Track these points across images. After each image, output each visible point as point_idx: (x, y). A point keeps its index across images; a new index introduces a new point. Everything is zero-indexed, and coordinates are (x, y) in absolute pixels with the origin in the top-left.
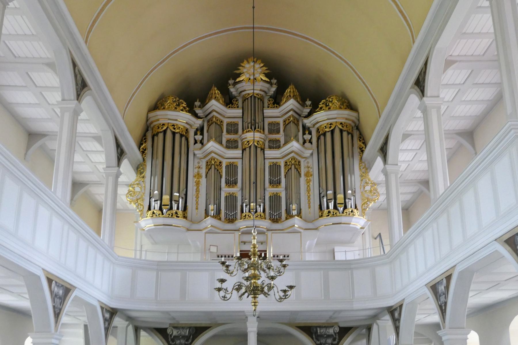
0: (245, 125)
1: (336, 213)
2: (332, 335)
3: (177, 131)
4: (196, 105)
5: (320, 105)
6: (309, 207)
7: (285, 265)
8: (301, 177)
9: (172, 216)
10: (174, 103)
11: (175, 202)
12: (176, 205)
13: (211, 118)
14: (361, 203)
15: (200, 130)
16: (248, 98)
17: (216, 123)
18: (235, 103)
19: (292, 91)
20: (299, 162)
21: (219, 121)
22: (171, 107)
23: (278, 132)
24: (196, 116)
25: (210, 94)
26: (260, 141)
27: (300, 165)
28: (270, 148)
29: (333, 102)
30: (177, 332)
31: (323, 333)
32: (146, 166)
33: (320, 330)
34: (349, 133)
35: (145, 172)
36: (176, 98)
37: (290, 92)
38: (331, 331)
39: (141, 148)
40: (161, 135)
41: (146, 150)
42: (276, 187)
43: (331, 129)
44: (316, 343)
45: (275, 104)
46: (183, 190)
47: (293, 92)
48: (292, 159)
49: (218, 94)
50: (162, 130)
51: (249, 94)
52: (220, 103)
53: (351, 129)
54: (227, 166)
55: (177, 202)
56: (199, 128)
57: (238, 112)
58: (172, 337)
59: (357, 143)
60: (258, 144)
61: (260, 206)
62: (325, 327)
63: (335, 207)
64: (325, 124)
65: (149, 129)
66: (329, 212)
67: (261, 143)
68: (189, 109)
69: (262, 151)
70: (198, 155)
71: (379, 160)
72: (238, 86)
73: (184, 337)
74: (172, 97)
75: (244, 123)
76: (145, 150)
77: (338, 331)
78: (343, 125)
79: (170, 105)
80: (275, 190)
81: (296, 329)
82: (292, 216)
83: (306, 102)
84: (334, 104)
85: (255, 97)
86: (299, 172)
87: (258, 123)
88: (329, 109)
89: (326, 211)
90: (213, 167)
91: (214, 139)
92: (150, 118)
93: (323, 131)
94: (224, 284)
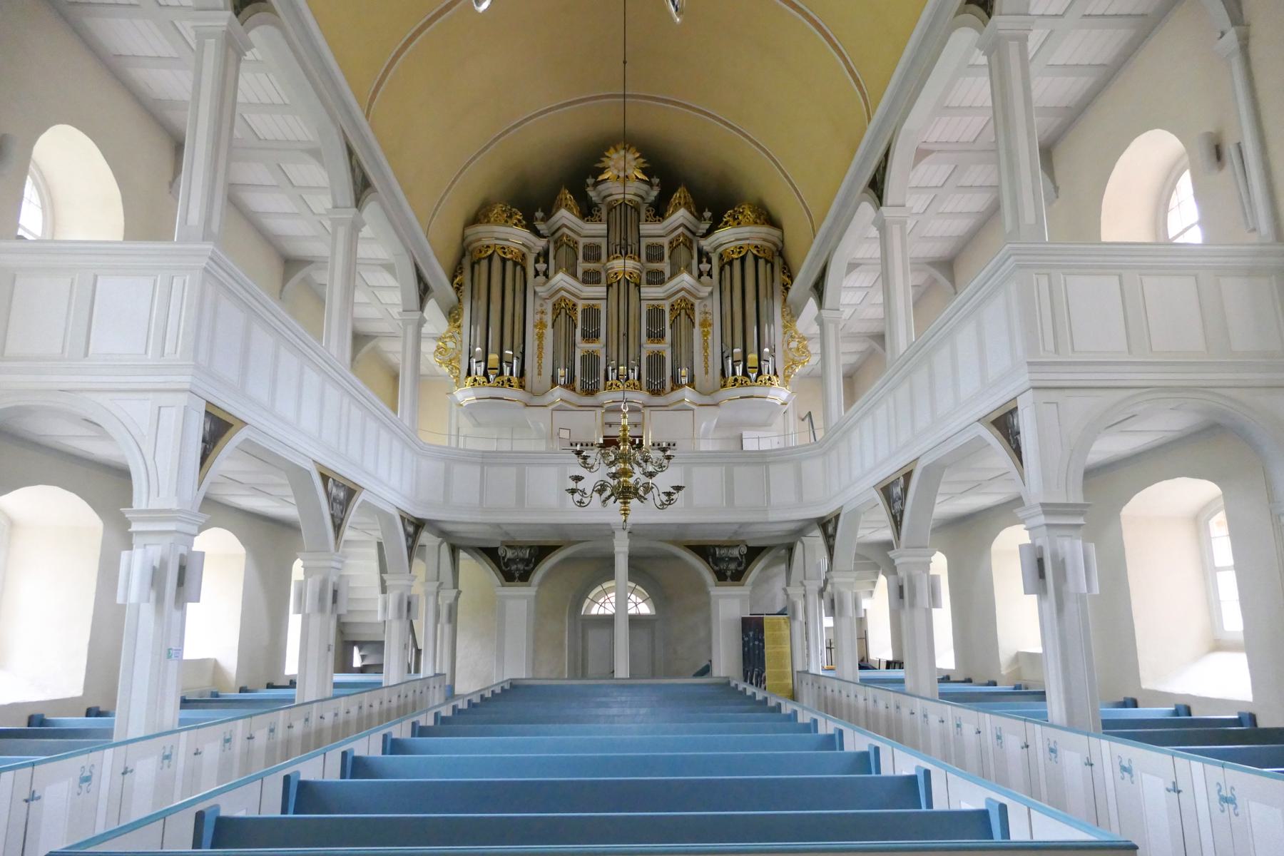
0: (612, 248)
1: (746, 382)
2: (737, 558)
3: (509, 256)
6: (707, 373)
9: (502, 385)
12: (508, 368)
13: (559, 238)
15: (544, 256)
17: (567, 245)
19: (682, 196)
23: (661, 259)
24: (537, 233)
28: (650, 283)
29: (745, 213)
30: (513, 554)
32: (463, 310)
34: (767, 261)
37: (680, 197)
38: (735, 553)
39: (455, 281)
40: (484, 263)
43: (741, 255)
46: (519, 347)
47: (685, 197)
48: (681, 301)
49: (571, 200)
50: (485, 255)
52: (573, 213)
54: (584, 311)
55: (510, 364)
56: (542, 252)
57: (600, 228)
58: (506, 560)
59: (779, 277)
60: (630, 277)
61: (633, 370)
63: (745, 373)
65: (467, 253)
66: (736, 380)
71: (812, 303)
72: (600, 187)
73: (522, 560)
74: (500, 203)
76: (461, 285)
79: (497, 217)
80: (655, 347)
82: (681, 386)
83: (704, 214)
85: (626, 204)
86: (691, 320)
88: (739, 224)
89: (731, 379)
90: (563, 311)
94: (579, 483)
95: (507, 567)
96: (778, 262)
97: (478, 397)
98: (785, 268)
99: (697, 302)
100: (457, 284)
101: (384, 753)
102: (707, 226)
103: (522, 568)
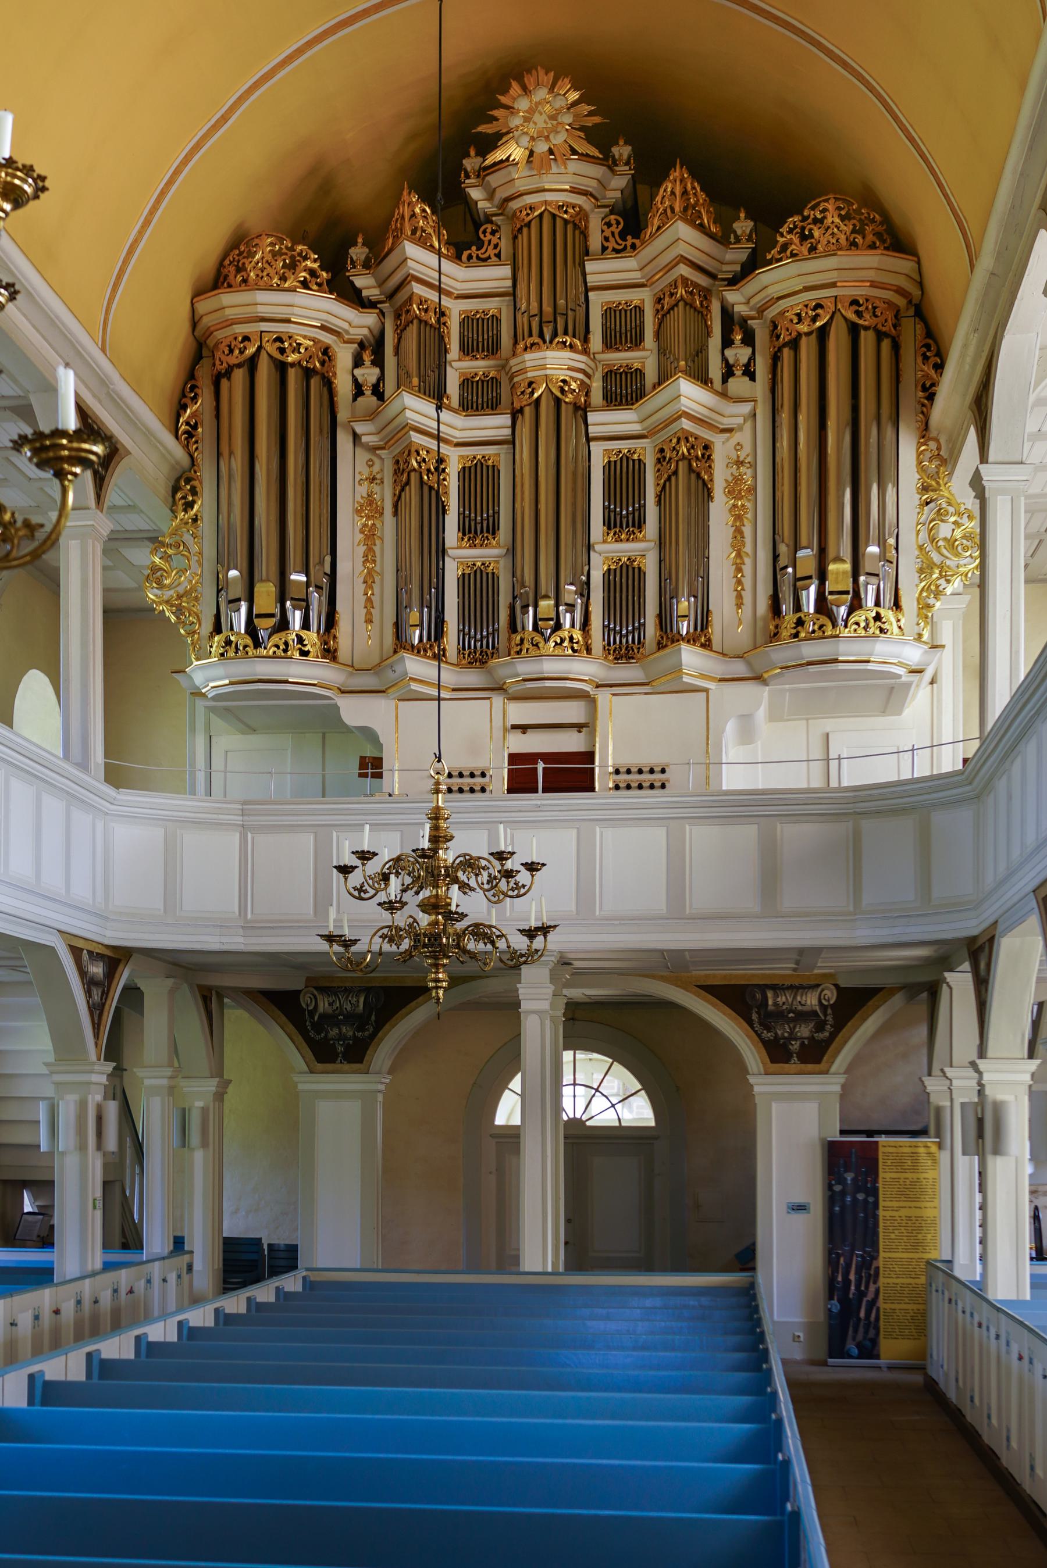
0: (522, 320)
2: (814, 1013)
3: (292, 358)
4: (355, 258)
5: (782, 235)
7: (512, 871)
8: (712, 498)
10: (276, 260)
11: (294, 602)
12: (298, 613)
14: (917, 586)
16: (530, 221)
17: (420, 321)
18: (490, 242)
19: (678, 190)
20: (706, 447)
21: (432, 314)
22: (268, 275)
23: (637, 341)
24: (354, 298)
25: (397, 219)
26: (572, 378)
27: (709, 456)
29: (829, 220)
30: (330, 1004)
31: (784, 1007)
33: (776, 996)
35: (199, 503)
36: (281, 240)
37: (673, 193)
38: (811, 1000)
39: (181, 420)
40: (239, 376)
41: (199, 426)
42: (628, 540)
43: (818, 324)
44: (759, 1036)
45: (629, 238)
47: (685, 193)
50: (242, 358)
51: (532, 208)
53: (889, 319)
58: (316, 1018)
61: (571, 607)
62: (791, 987)
63: (823, 606)
64: (798, 304)
65: (205, 352)
67: (574, 386)
68: (330, 275)
69: (580, 412)
70: (364, 439)
72: (494, 180)
75: (519, 316)
76: (195, 427)
77: (832, 1002)
78: (860, 309)
80: (625, 549)
81: (694, 993)
82: (677, 639)
84: (830, 231)
85: (554, 216)
86: (704, 484)
87: (566, 315)
88: (813, 249)
91: (415, 381)
92: (202, 317)
93: (791, 334)
95: (319, 1033)
96: (911, 334)
97: (233, 679)
98: (928, 347)
99: (718, 441)
100: (188, 424)
101: (31, 1402)
102: (743, 256)
103: (351, 1033)
